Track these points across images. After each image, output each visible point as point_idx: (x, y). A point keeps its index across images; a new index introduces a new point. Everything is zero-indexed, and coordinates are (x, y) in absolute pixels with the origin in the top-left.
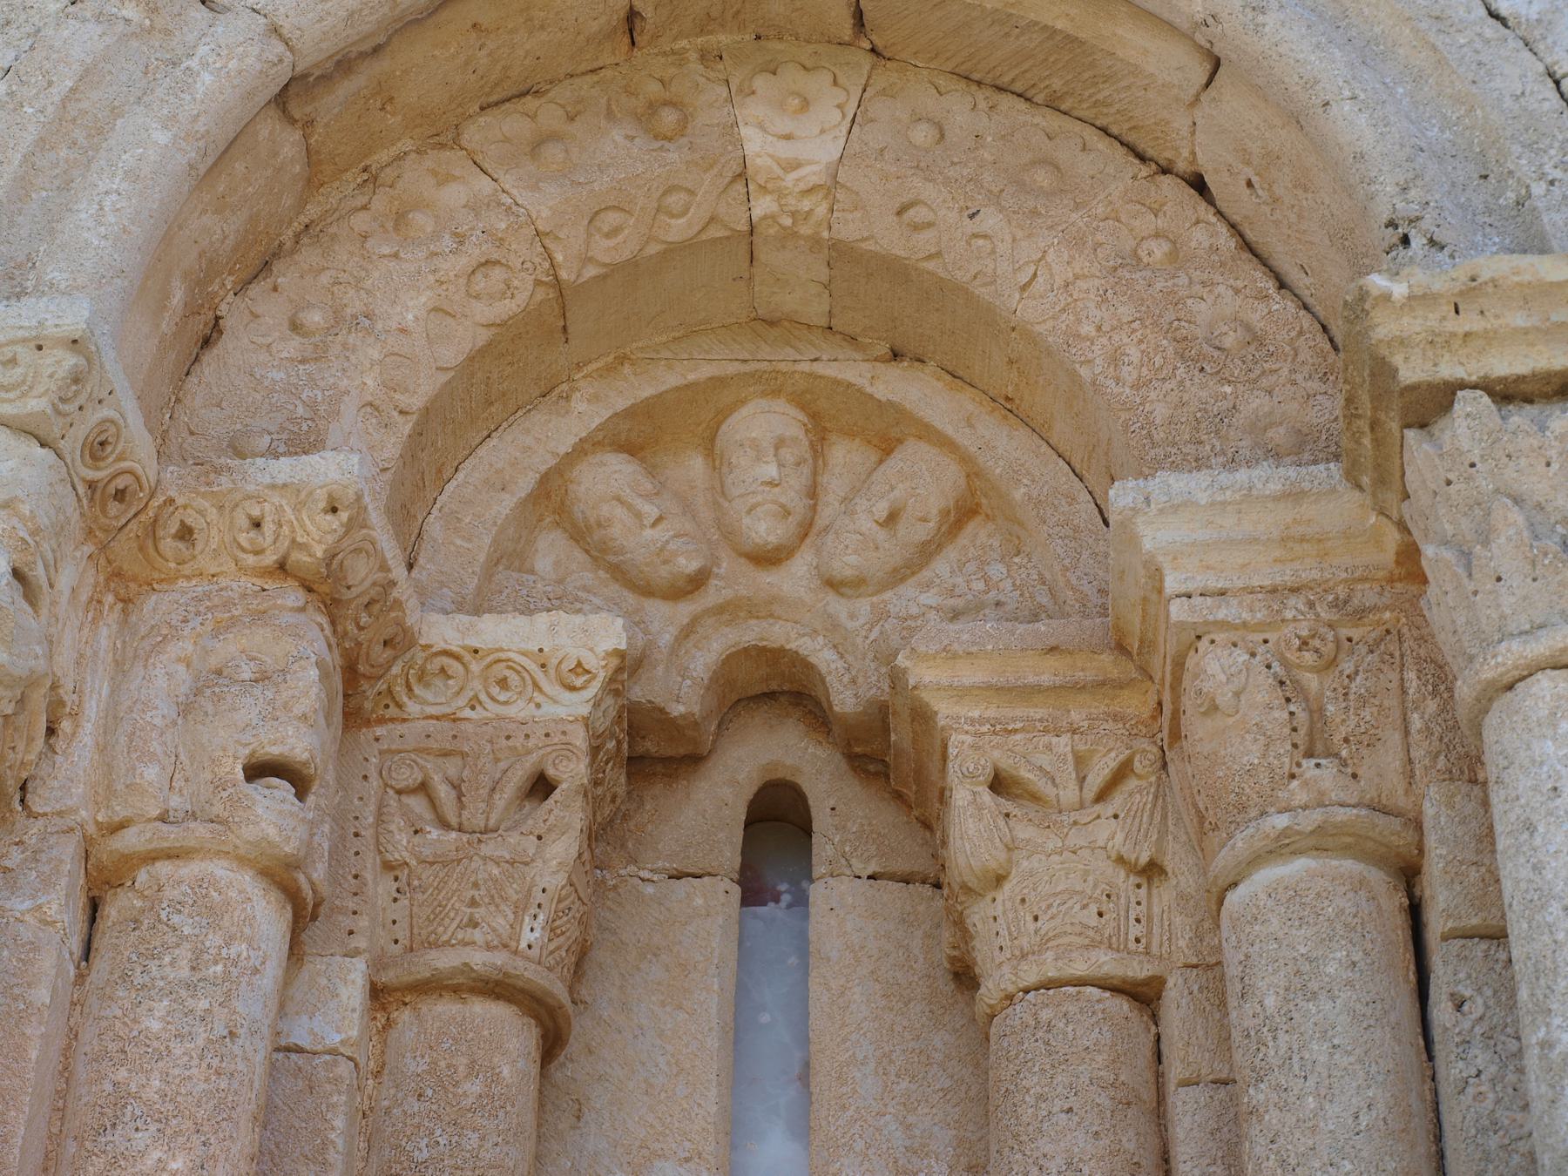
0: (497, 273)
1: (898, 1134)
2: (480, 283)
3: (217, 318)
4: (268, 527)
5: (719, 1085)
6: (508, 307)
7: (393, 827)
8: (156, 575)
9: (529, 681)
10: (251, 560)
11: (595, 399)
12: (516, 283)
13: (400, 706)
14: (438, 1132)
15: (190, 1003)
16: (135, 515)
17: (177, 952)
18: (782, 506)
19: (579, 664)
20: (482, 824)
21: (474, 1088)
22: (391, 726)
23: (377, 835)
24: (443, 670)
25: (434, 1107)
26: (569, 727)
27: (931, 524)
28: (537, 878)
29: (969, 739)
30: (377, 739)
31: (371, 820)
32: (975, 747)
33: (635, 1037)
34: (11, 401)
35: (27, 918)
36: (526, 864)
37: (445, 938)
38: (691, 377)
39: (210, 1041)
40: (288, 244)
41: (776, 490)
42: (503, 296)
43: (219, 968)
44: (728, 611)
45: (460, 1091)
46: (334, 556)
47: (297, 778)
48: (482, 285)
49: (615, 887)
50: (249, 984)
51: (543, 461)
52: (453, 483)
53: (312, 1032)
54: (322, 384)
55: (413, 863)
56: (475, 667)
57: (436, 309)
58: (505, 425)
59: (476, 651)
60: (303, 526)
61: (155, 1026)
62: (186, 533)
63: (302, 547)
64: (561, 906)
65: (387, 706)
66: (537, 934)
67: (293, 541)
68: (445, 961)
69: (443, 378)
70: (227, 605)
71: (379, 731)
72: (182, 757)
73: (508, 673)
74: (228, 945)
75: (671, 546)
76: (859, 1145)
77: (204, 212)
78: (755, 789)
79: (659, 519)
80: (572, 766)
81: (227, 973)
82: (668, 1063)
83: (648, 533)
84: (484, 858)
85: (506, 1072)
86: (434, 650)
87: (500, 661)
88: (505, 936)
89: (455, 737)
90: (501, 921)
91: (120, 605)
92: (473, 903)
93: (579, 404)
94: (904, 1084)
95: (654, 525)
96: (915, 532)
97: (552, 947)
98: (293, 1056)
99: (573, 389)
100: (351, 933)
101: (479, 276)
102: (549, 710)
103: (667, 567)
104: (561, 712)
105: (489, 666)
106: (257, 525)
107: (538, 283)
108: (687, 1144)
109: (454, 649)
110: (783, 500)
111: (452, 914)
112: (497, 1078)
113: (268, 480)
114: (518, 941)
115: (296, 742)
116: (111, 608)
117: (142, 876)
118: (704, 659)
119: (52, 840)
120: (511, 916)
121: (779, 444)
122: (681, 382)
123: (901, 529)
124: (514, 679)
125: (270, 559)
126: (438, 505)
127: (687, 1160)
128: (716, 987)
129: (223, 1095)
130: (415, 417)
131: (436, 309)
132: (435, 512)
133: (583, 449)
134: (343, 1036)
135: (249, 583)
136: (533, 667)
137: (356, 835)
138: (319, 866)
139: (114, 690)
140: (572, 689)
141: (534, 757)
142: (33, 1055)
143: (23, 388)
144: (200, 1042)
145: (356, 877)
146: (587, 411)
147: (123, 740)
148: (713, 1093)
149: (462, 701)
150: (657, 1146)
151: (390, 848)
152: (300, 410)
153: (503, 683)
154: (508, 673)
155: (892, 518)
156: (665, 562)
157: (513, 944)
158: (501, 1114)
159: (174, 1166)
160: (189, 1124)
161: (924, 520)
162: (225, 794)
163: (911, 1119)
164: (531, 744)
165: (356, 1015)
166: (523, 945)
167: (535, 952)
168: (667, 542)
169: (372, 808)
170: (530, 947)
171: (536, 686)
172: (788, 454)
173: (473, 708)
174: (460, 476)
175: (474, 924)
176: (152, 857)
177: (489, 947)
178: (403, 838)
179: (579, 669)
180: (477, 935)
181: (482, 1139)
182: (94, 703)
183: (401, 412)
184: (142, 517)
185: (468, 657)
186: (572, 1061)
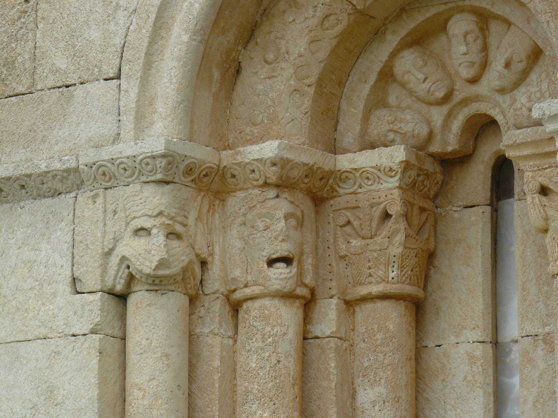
0: (332, 18)
1: (544, 309)
2: (326, 24)
3: (240, 62)
4: (257, 173)
5: (484, 295)
6: (340, 28)
7: (340, 243)
8: (230, 190)
9: (376, 177)
10: (255, 183)
11: (394, 32)
12: (340, 18)
13: (337, 191)
14: (370, 355)
15: (263, 355)
16: (216, 175)
17: (257, 336)
18: (470, 62)
19: (391, 168)
20: (370, 235)
21: (380, 336)
22: (336, 199)
23: (335, 246)
24: (347, 177)
25: (368, 345)
26: (394, 191)
27: (524, 63)
28: (391, 253)
29: (531, 174)
30: (331, 206)
31: (332, 241)
32: (533, 177)
33: (455, 280)
34: (152, 176)
35: (209, 334)
36: (386, 249)
37: (363, 281)
38: (428, 15)
39: (271, 367)
40: (259, 20)
41: (467, 56)
42: (337, 24)
43: (271, 339)
44: (465, 102)
45: (376, 338)
46: (282, 177)
47: (287, 260)
48: (327, 25)
49: (445, 215)
50: (282, 341)
51: (377, 67)
52: (348, 82)
53: (321, 331)
54: (275, 89)
55: (349, 254)
56: (357, 175)
57: (312, 41)
58: (363, 51)
59: (356, 169)
60: (267, 171)
61: (254, 365)
62: (233, 176)
63: (269, 178)
64: (404, 258)
65: (333, 192)
66: (395, 273)
67: (266, 176)
68: (363, 291)
69: (322, 65)
70: (252, 199)
71: (332, 202)
72: (249, 260)
73: (368, 175)
74: (272, 329)
75: (432, 89)
76: (530, 316)
77: (218, 36)
78: (493, 161)
79: (425, 79)
80: (395, 208)
81: (274, 340)
82: (466, 289)
83: (423, 86)
84: (370, 251)
85: (391, 327)
86: (342, 171)
87: (364, 172)
88: (383, 277)
89: (356, 200)
90: (381, 272)
91: (221, 203)
92: (369, 268)
93: (389, 37)
94: (546, 288)
95: (424, 81)
96: (518, 67)
97: (403, 273)
98: (317, 340)
99: (386, 29)
100: (330, 289)
101: (325, 22)
102: (385, 185)
103: (433, 96)
104: (390, 185)
105: (361, 174)
106: (253, 171)
107: (349, 14)
108: (473, 322)
109: (349, 170)
110: (470, 60)
111: (363, 273)
112: (388, 330)
113: (252, 158)
114: (388, 278)
115: (282, 249)
116: (218, 205)
117: (245, 307)
118: (457, 125)
119: (212, 304)
120: (384, 269)
121: (466, 34)
122: (424, 18)
123: (513, 67)
124: (371, 177)
125: (261, 182)
126: (344, 94)
127: (474, 329)
128: (480, 255)
129: (278, 385)
130: (314, 85)
131: (312, 41)
132: (343, 97)
133: (393, 55)
134: (331, 331)
135: (257, 191)
136: (376, 171)
137: (328, 248)
138: (308, 277)
139: (224, 240)
140: (392, 177)
141: (382, 206)
142: (217, 385)
143: (153, 171)
144: (268, 369)
145: (330, 265)
146: (392, 40)
147: (228, 261)
148: (481, 300)
149: (356, 187)
150: (464, 324)
151: (340, 251)
152: (270, 102)
153: (368, 178)
154: (368, 175)
155: (507, 65)
156: (431, 95)
157: (387, 279)
158: (391, 344)
159: (265, 415)
160: (268, 399)
161: (521, 61)
162: (262, 276)
163: (548, 302)
164: (381, 200)
165: (334, 322)
166: (390, 279)
167: (395, 280)
168: (430, 88)
169: (332, 236)
170: (393, 278)
171: (379, 177)
172: (470, 38)
173: (361, 188)
174: (350, 78)
175: (370, 275)
176: (246, 300)
177: (378, 283)
178: (343, 247)
179: (391, 170)
180: (373, 279)
181: (385, 355)
182: (217, 247)
183: (309, 86)
184: (218, 174)
185: (354, 172)
186: (434, 292)
